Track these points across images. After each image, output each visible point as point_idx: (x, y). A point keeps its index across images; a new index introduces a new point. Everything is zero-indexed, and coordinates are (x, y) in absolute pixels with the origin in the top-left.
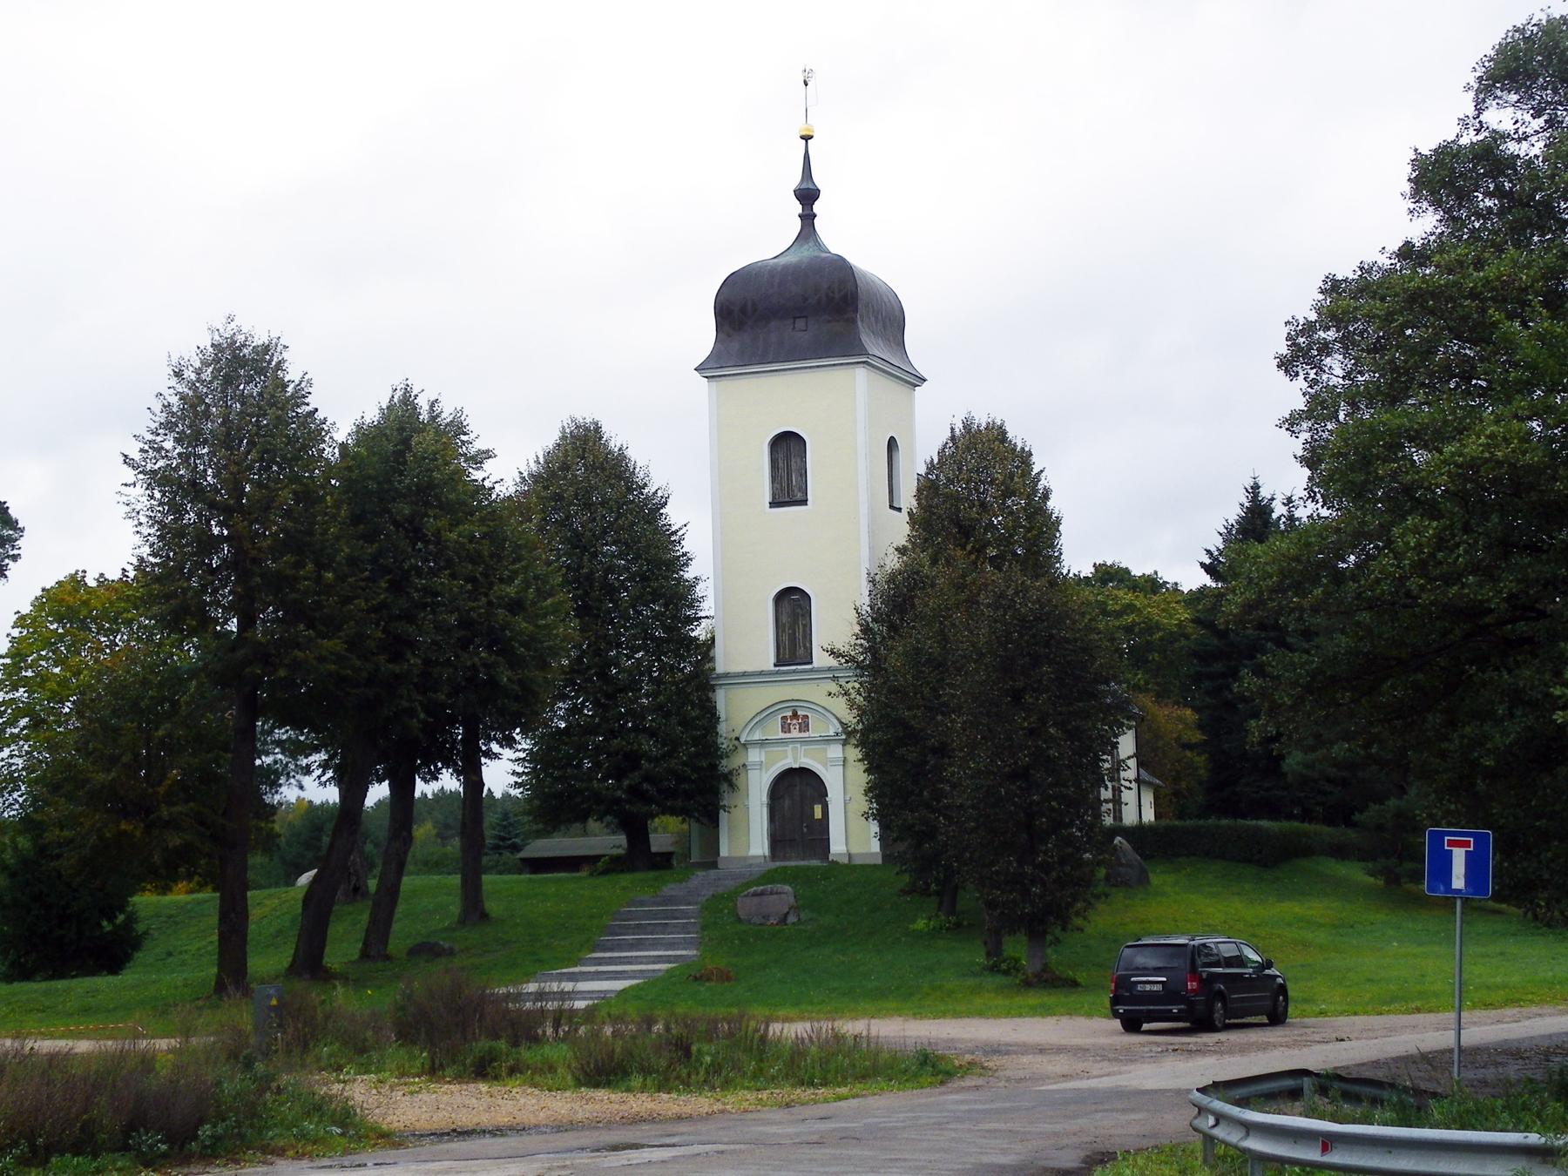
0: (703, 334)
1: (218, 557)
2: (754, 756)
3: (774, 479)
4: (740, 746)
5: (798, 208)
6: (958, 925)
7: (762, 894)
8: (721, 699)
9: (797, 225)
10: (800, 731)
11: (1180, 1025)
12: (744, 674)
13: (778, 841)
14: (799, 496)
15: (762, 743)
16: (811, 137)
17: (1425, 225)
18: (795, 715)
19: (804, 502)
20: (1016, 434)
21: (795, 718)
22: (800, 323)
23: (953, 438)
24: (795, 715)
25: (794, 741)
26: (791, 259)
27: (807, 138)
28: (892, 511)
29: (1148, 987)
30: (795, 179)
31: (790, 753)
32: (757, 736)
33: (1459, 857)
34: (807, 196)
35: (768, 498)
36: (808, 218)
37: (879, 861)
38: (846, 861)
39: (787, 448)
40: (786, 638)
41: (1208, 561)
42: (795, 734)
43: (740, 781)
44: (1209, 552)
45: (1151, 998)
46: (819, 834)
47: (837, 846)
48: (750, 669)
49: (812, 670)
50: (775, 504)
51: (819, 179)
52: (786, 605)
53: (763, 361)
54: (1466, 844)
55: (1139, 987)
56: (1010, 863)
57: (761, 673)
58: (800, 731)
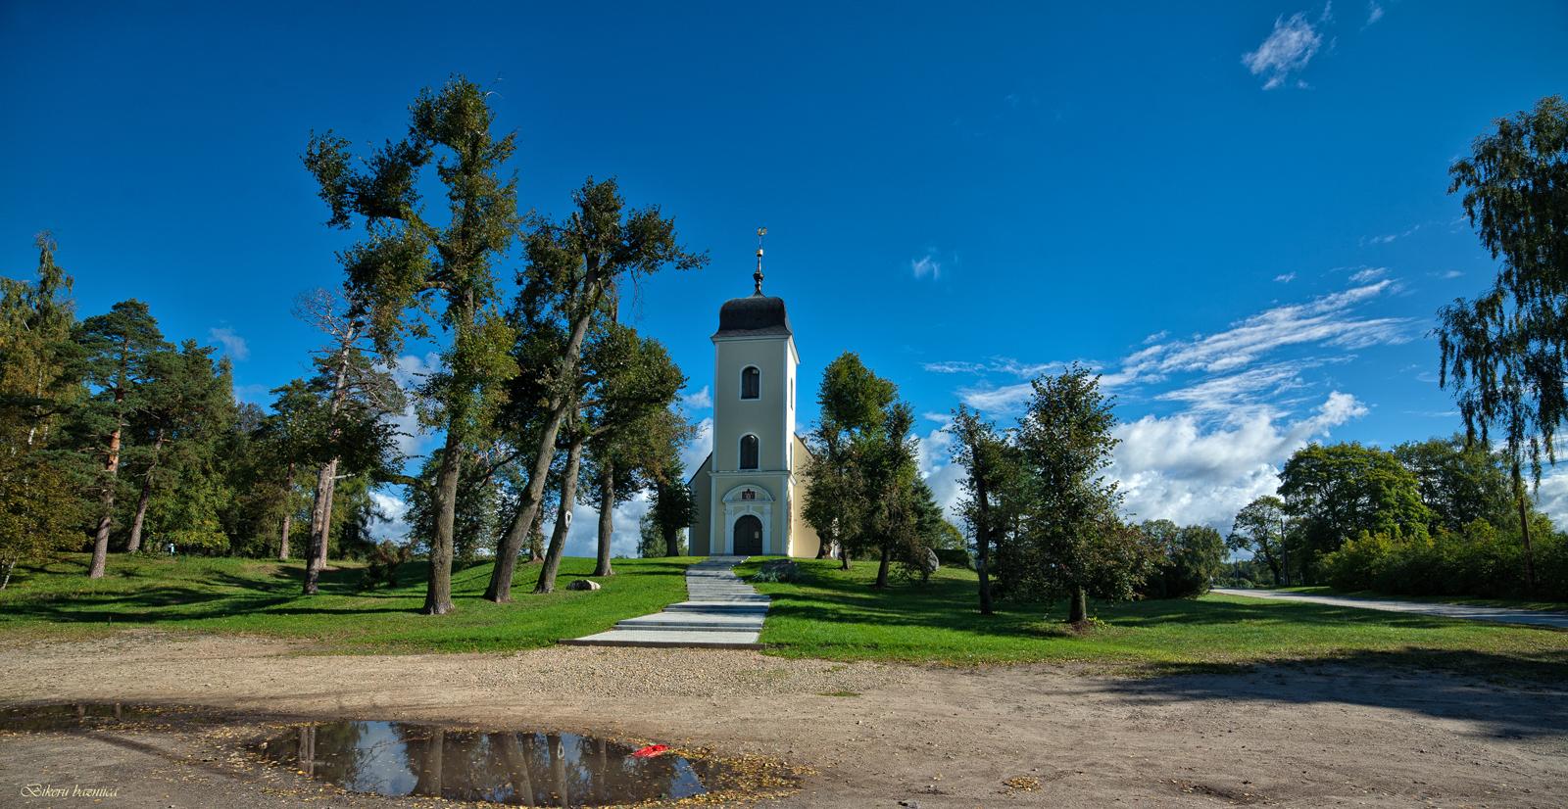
19: (757, 397)
35: (740, 395)
50: (743, 397)
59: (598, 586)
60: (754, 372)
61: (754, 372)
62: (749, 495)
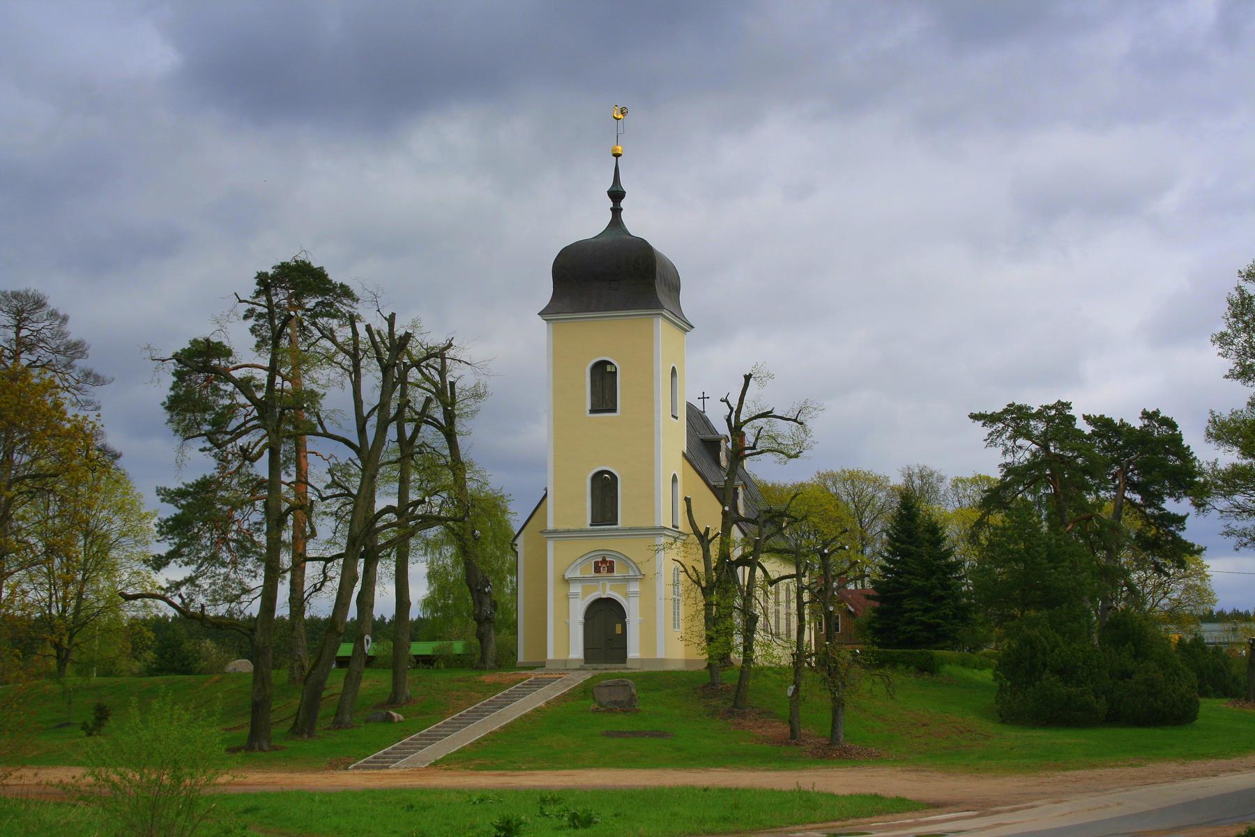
0: (545, 290)
1: (1132, 471)
5: (611, 204)
9: (608, 216)
10: (608, 572)
11: (976, 813)
16: (620, 155)
17: (190, 346)
19: (614, 410)
27: (617, 156)
28: (673, 419)
34: (617, 195)
35: (589, 407)
36: (616, 211)
39: (603, 376)
48: (571, 527)
49: (617, 529)
50: (593, 411)
51: (625, 185)
53: (597, 310)
57: (580, 531)
58: (608, 572)
59: (401, 717)
60: (609, 368)
61: (609, 368)
62: (604, 565)
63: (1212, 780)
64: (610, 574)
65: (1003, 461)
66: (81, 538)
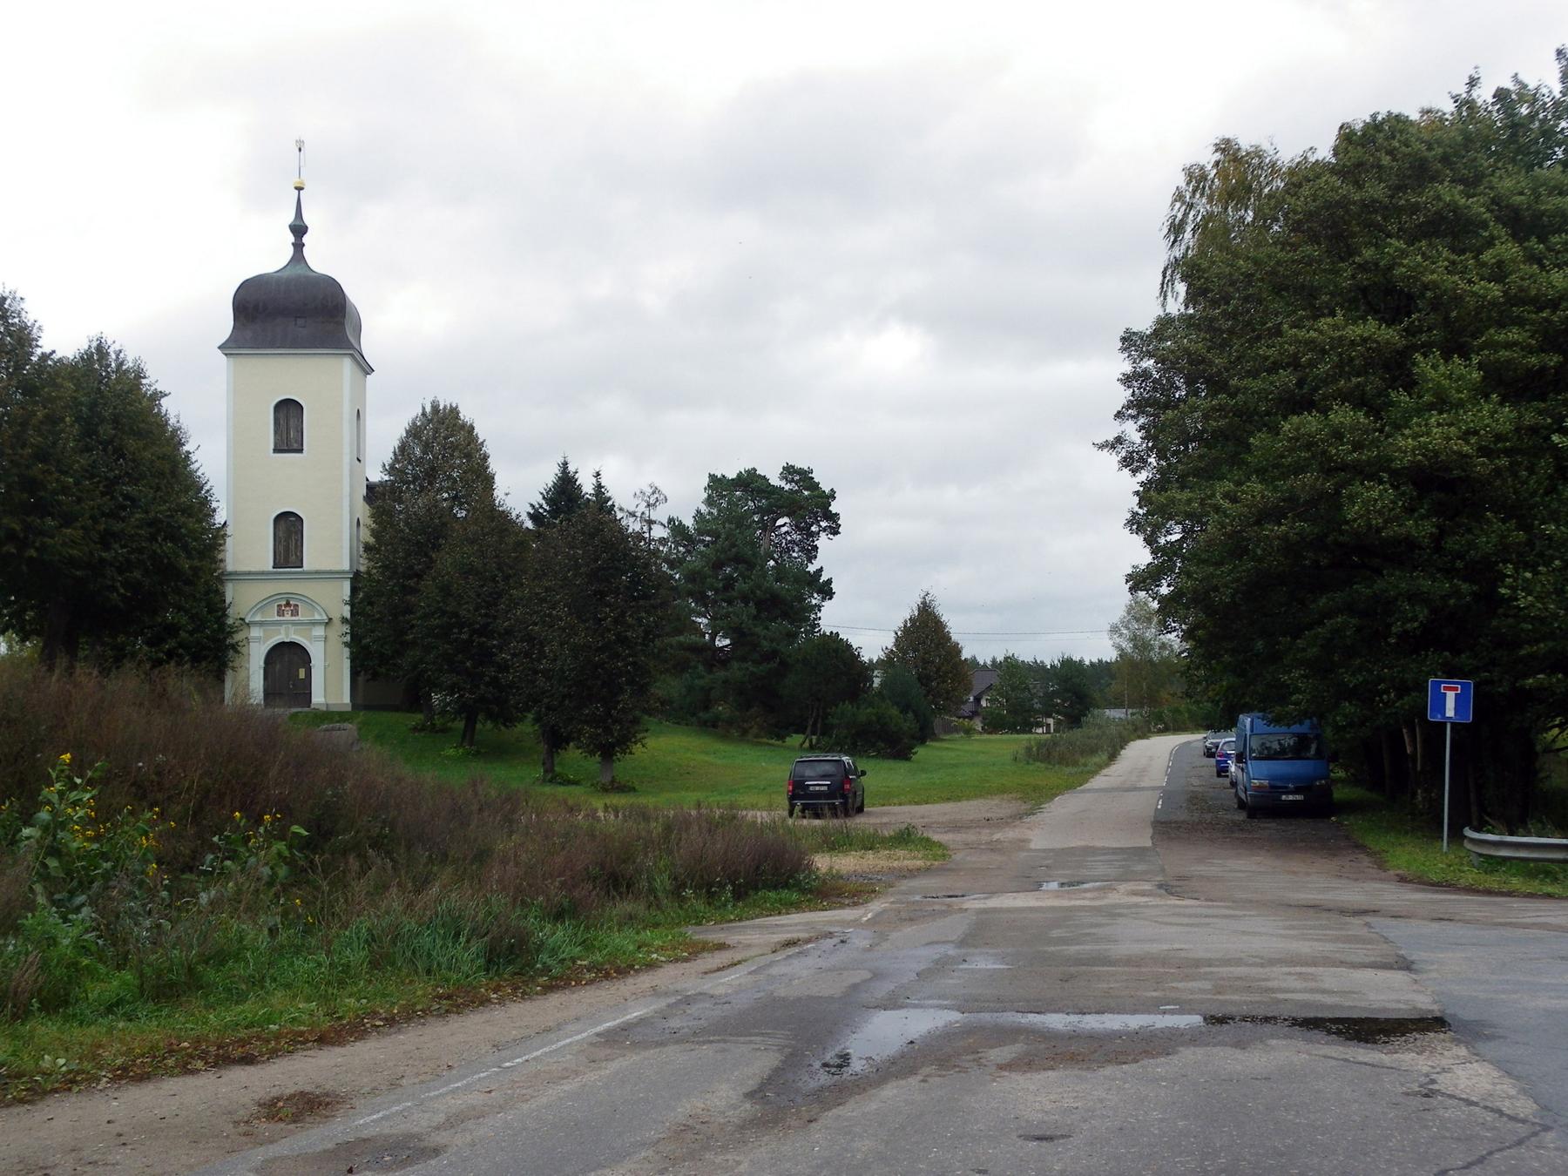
0: (224, 323)
2: (255, 632)
3: (276, 432)
4: (245, 624)
5: (291, 238)
6: (478, 752)
7: (333, 729)
8: (230, 591)
9: (290, 251)
12: (249, 573)
13: (272, 692)
14: (295, 446)
15: (261, 624)
16: (302, 189)
18: (288, 604)
19: (301, 451)
20: (466, 415)
21: (288, 605)
22: (300, 322)
23: (424, 414)
24: (288, 604)
25: (287, 622)
26: (286, 274)
27: (299, 189)
29: (817, 788)
30: (290, 217)
31: (283, 631)
32: (258, 618)
33: (1450, 698)
34: (299, 230)
36: (298, 246)
37: (349, 709)
38: (325, 709)
39: (288, 412)
40: (281, 548)
41: (532, 512)
42: (288, 617)
43: (244, 650)
44: (532, 505)
45: (818, 795)
46: (303, 692)
47: (318, 698)
48: (253, 570)
50: (276, 450)
51: (307, 218)
52: (282, 524)
53: (272, 345)
54: (1456, 689)
55: (811, 788)
56: (597, 708)
57: (263, 573)
63: (917, 807)
64: (294, 618)
65: (1119, 458)
66: (187, 658)
